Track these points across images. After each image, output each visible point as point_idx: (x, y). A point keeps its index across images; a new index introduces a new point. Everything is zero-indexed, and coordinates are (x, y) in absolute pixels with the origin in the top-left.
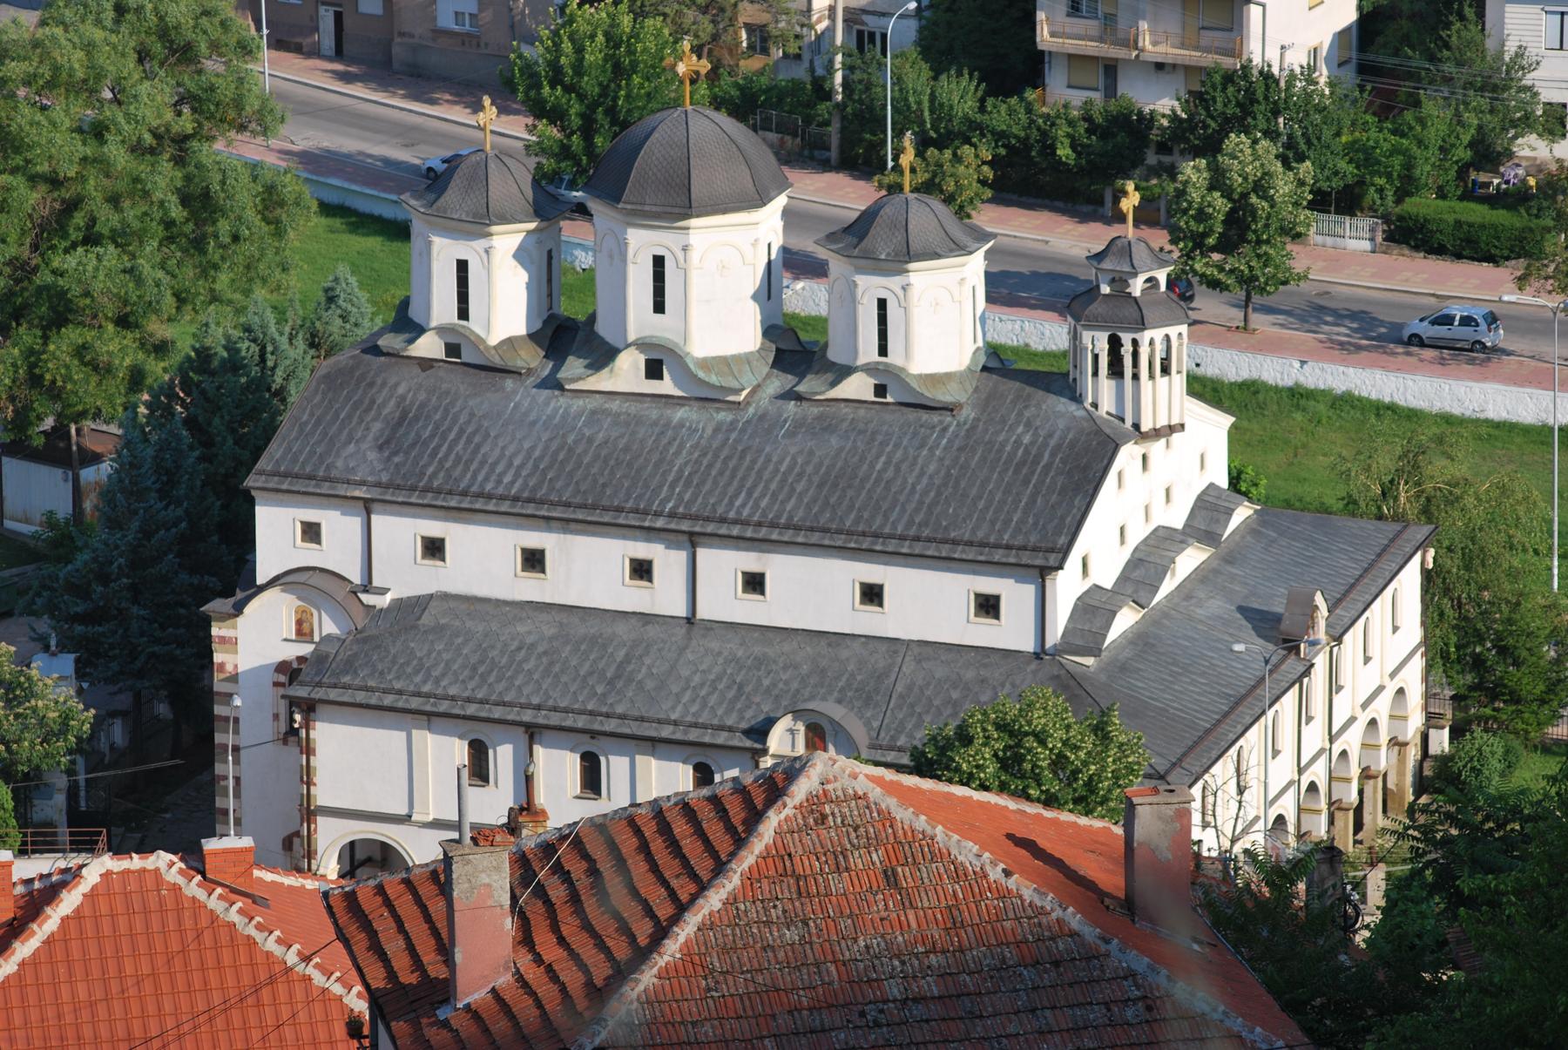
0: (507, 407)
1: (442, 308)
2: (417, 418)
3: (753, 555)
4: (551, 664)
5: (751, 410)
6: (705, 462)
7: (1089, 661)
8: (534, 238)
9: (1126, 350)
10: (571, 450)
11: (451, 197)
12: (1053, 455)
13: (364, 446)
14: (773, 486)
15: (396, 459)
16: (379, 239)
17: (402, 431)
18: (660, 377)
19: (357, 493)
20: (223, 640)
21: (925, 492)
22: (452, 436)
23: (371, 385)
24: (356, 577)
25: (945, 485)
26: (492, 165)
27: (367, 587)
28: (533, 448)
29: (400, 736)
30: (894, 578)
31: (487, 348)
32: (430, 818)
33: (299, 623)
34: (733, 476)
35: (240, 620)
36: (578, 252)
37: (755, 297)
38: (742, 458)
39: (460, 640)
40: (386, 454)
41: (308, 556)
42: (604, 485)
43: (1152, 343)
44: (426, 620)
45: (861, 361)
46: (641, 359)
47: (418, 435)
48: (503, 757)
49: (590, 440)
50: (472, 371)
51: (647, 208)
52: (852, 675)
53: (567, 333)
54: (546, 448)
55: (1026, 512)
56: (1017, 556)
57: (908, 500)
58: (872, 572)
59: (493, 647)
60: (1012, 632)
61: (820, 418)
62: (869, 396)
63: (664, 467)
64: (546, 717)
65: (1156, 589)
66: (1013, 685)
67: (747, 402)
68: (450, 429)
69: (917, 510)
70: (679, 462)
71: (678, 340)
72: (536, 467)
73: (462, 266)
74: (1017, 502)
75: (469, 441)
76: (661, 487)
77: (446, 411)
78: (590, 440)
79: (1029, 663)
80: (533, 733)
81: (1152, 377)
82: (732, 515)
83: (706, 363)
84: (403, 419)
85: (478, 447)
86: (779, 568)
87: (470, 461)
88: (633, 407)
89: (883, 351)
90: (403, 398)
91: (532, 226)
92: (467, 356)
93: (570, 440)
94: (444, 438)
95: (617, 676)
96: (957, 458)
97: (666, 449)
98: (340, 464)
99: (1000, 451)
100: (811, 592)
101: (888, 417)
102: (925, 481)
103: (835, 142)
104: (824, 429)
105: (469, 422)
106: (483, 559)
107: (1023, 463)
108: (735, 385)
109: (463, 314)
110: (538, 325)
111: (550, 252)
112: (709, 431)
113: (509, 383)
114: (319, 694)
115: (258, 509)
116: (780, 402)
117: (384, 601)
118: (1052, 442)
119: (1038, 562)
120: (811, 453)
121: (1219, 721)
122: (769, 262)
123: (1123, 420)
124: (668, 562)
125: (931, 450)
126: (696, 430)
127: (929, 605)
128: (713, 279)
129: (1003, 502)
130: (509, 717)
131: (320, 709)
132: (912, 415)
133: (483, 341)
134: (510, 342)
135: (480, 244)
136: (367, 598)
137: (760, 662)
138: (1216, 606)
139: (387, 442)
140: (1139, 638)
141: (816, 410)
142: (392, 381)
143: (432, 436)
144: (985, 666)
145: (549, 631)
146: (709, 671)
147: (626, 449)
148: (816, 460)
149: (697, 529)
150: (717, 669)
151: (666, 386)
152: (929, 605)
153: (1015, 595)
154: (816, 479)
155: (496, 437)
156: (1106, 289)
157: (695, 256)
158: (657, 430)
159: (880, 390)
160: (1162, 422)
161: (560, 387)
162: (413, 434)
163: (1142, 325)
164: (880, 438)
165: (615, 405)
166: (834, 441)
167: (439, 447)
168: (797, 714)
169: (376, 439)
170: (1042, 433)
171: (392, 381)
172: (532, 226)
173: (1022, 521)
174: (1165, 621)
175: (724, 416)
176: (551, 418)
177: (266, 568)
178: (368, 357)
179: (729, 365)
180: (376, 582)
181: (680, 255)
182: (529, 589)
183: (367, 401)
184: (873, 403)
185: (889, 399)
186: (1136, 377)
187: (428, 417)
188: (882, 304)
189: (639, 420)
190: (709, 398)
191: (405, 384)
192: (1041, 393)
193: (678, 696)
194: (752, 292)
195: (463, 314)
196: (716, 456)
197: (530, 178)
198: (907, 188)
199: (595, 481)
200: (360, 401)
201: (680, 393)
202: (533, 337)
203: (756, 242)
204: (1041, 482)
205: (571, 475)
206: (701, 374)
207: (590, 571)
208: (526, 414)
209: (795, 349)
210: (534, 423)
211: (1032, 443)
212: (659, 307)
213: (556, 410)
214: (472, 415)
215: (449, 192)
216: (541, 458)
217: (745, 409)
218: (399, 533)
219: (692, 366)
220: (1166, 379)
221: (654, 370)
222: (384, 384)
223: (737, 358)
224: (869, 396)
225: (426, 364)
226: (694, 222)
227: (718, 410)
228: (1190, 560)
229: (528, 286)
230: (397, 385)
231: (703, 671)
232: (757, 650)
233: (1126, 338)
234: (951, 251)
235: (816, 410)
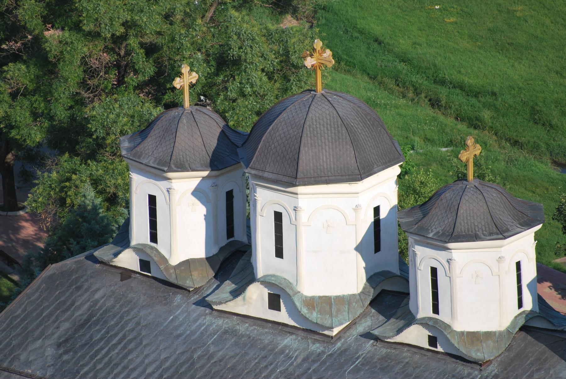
0: (166, 319)
1: (139, 232)
2: (97, 322)
5: (339, 344)
8: (210, 182)
10: (193, 364)
13: (48, 342)
18: (279, 309)
22: (114, 342)
23: (78, 288)
26: (184, 121)
28: (166, 359)
40: (61, 351)
46: (265, 292)
47: (91, 338)
50: (157, 284)
51: (266, 175)
53: (232, 259)
61: (385, 358)
62: (425, 344)
68: (116, 335)
71: (292, 280)
73: (152, 200)
75: (124, 348)
77: (121, 318)
83: (311, 302)
84: (85, 324)
85: (130, 352)
87: (117, 365)
89: (436, 310)
90: (96, 302)
91: (205, 173)
92: (154, 273)
93: (195, 356)
94: (108, 343)
105: (132, 330)
109: (154, 238)
110: (215, 251)
111: (230, 195)
112: (299, 360)
113: (178, 298)
116: (363, 339)
122: (377, 223)
126: (291, 358)
132: (452, 364)
133: (165, 260)
134: (188, 264)
135: (163, 184)
139: (66, 341)
142: (94, 288)
143: (101, 339)
155: (145, 346)
158: (263, 353)
159: (433, 341)
162: (88, 336)
165: (243, 328)
167: (102, 348)
169: (59, 338)
171: (94, 288)
172: (205, 173)
175: (316, 347)
176: (193, 333)
178: (89, 262)
179: (331, 305)
181: (292, 213)
183: (68, 303)
184: (428, 350)
185: (439, 349)
187: (106, 322)
188: (434, 271)
189: (253, 342)
190: (312, 332)
191: (102, 291)
192: (557, 358)
194: (355, 246)
195: (154, 238)
198: (471, 176)
200: (64, 302)
201: (292, 323)
202: (209, 259)
206: (304, 311)
208: (177, 328)
209: (390, 294)
210: (179, 336)
212: (279, 253)
213: (200, 326)
214: (138, 324)
215: (149, 139)
216: (168, 369)
217: (334, 344)
219: (298, 304)
221: (274, 302)
222: (89, 288)
223: (340, 300)
224: (425, 344)
225: (126, 274)
226: (300, 189)
229: (206, 217)
234: (491, 234)
235: (384, 351)
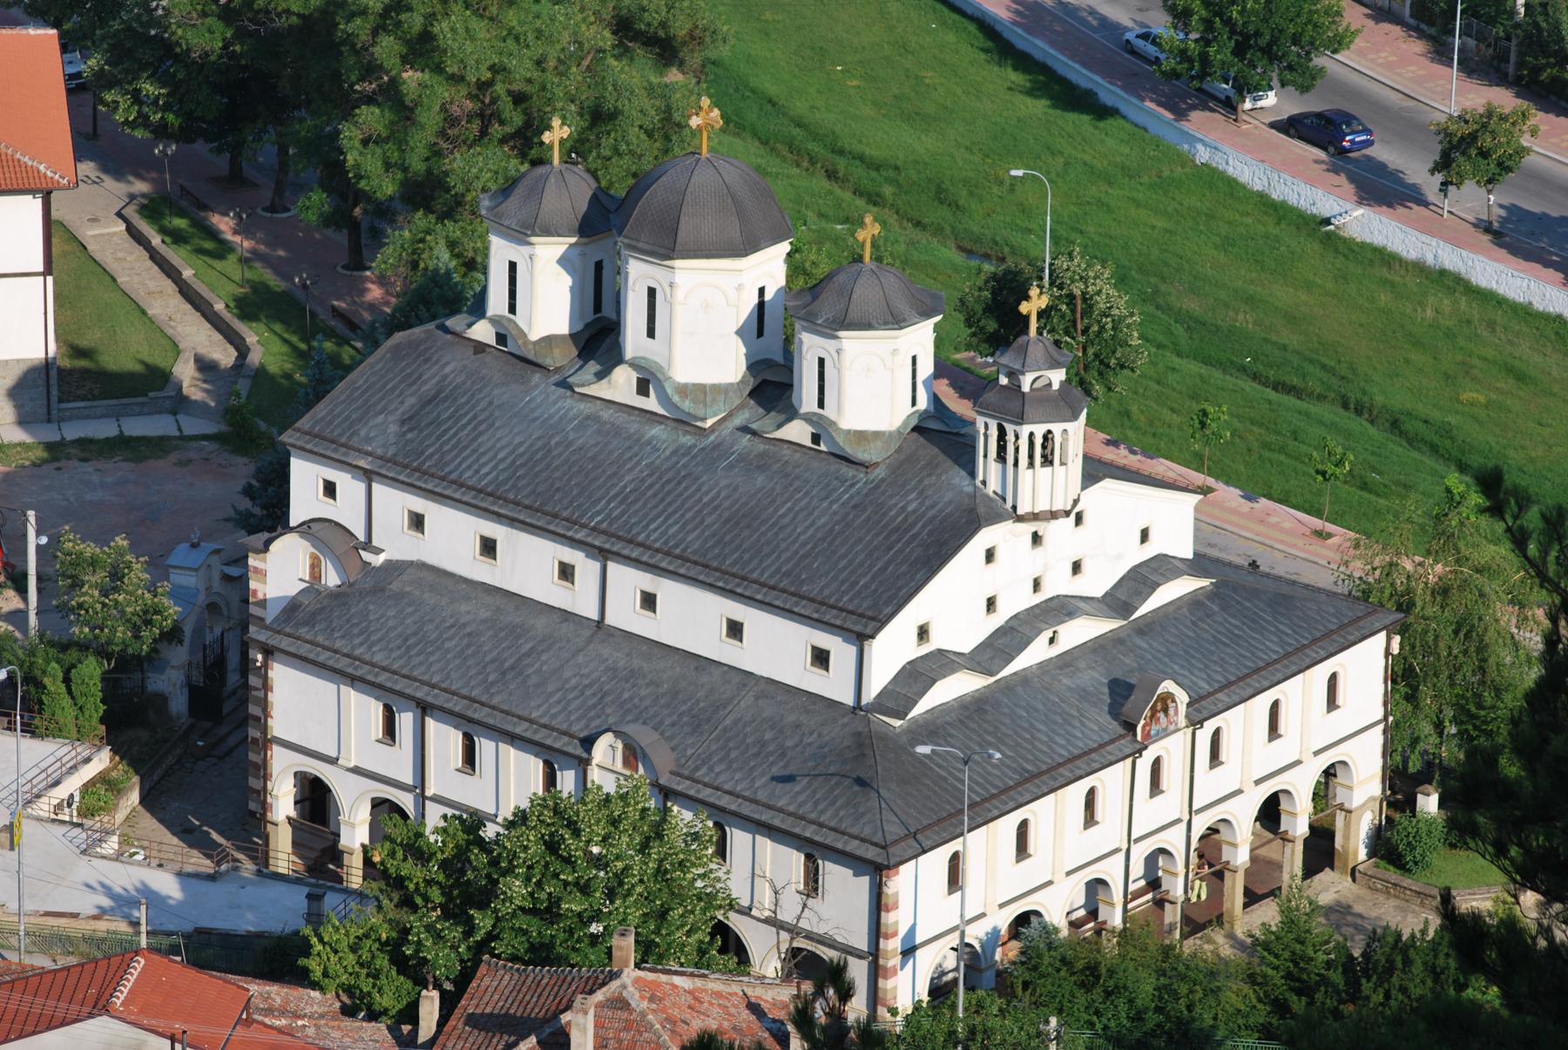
1: (497, 302)
3: (649, 576)
4: (468, 646)
5: (712, 438)
6: (649, 482)
7: (897, 723)
8: (576, 251)
9: (1010, 437)
10: (549, 451)
11: (513, 202)
12: (924, 527)
14: (688, 516)
15: (409, 436)
16: (1045, 102)
17: (428, 408)
19: (362, 463)
20: (256, 569)
21: (804, 544)
24: (362, 537)
25: (823, 539)
27: (368, 545)
28: (521, 444)
29: (332, 687)
30: (755, 620)
31: (527, 342)
32: (352, 765)
33: (312, 567)
34: (662, 500)
35: (268, 556)
36: (1200, 147)
37: (739, 333)
38: (679, 483)
39: (410, 610)
41: (326, 509)
42: (558, 489)
43: (1031, 434)
44: (395, 586)
45: (803, 410)
46: (634, 376)
47: (438, 416)
48: (406, 721)
49: (570, 444)
52: (698, 701)
53: (598, 337)
54: (531, 445)
55: (873, 579)
56: (844, 620)
57: (787, 549)
58: (739, 611)
59: (431, 621)
60: (835, 685)
61: (761, 455)
62: (808, 442)
63: (615, 480)
64: (436, 696)
65: (1010, 659)
66: (820, 735)
67: (713, 428)
69: (788, 560)
70: (628, 478)
71: (664, 365)
72: (514, 462)
74: (871, 566)
75: (475, 428)
76: (599, 500)
78: (570, 444)
79: (843, 716)
80: (424, 709)
81: (1031, 465)
82: (641, 538)
83: (684, 390)
85: (481, 434)
86: (670, 592)
87: (465, 448)
88: (620, 418)
89: (821, 404)
90: (445, 377)
91: (573, 240)
92: (511, 348)
95: (512, 668)
96: (848, 514)
97: (624, 464)
98: (363, 433)
99: (885, 514)
100: (690, 618)
101: (815, 464)
102: (810, 532)
103: (1513, 58)
104: (758, 467)
106: (451, 539)
107: (897, 529)
108: (700, 413)
110: (579, 327)
112: (668, 453)
113: (537, 377)
114: (285, 643)
115: (292, 460)
117: (378, 560)
118: (931, 513)
119: (858, 628)
120: (736, 489)
121: (994, 796)
122: (761, 305)
123: (1004, 499)
124: (587, 568)
125: (831, 504)
127: (776, 648)
128: (700, 315)
129: (861, 564)
130: (407, 691)
131: (277, 654)
132: (836, 465)
133: (525, 335)
134: (549, 340)
135: (525, 250)
136: (366, 556)
137: (633, 674)
138: (1094, 678)
139: (411, 418)
140: (972, 708)
141: (762, 447)
143: (449, 418)
144: (808, 712)
145: (484, 614)
146: (587, 676)
147: (593, 458)
148: (736, 495)
149: (607, 546)
150: (595, 675)
151: (651, 403)
152: (776, 648)
153: (841, 651)
154: (726, 514)
156: (1004, 381)
157: (680, 294)
158: (628, 443)
159: (816, 438)
160: (1042, 506)
161: (570, 388)
163: (1020, 419)
164: (797, 483)
165: (606, 414)
166: (760, 480)
167: (450, 428)
168: (618, 734)
170: (927, 503)
173: (866, 586)
174: (1019, 689)
175: (687, 440)
176: (551, 416)
177: (296, 517)
180: (375, 543)
182: (481, 571)
185: (823, 447)
186: (1016, 464)
187: (455, 399)
188: (821, 362)
190: (683, 422)
192: (949, 462)
193: (551, 694)
195: (512, 309)
196: (660, 477)
197: (591, 193)
199: (552, 485)
200: (410, 375)
201: (661, 411)
202: (573, 336)
203: (740, 287)
204: (901, 551)
205: (537, 474)
207: (529, 566)
209: (771, 384)
210: (536, 419)
211: (914, 512)
212: (651, 333)
214: (491, 403)
216: (522, 455)
218: (393, 503)
219: (669, 391)
220: (1049, 469)
221: (643, 388)
225: (480, 347)
226: (678, 263)
227: (686, 433)
228: (1078, 632)
229: (572, 289)
230: (447, 363)
231: (583, 676)
232: (637, 662)
233: (1010, 428)
234: (886, 323)
235: (762, 447)
